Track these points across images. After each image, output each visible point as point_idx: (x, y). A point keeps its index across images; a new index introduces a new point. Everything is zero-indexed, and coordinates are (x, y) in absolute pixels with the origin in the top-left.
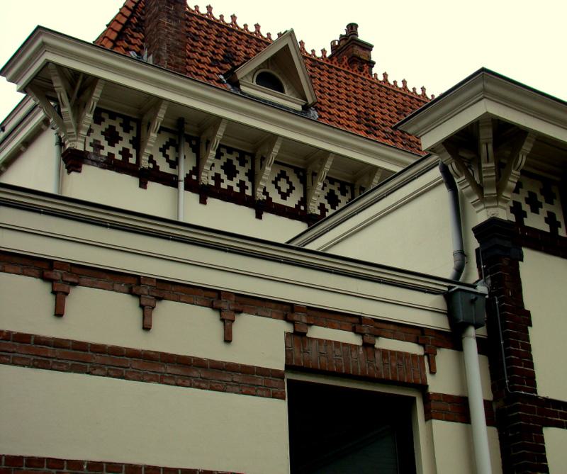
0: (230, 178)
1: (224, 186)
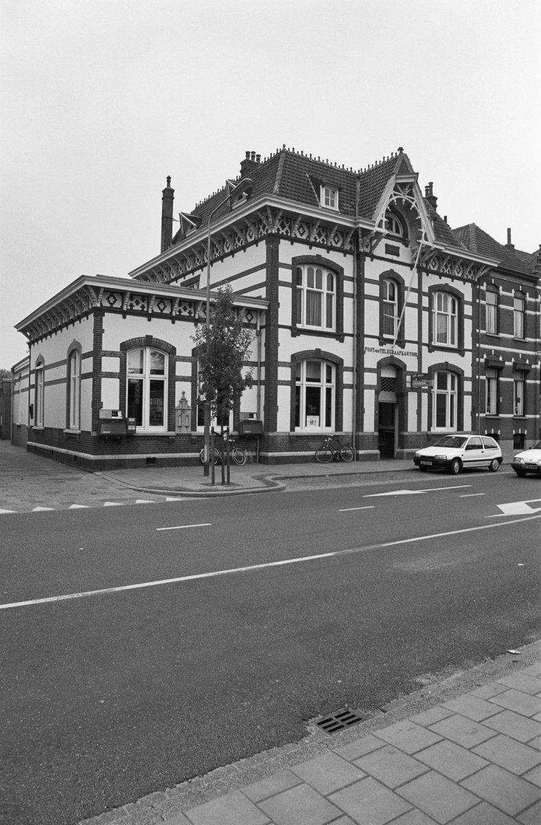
0: (283, 229)
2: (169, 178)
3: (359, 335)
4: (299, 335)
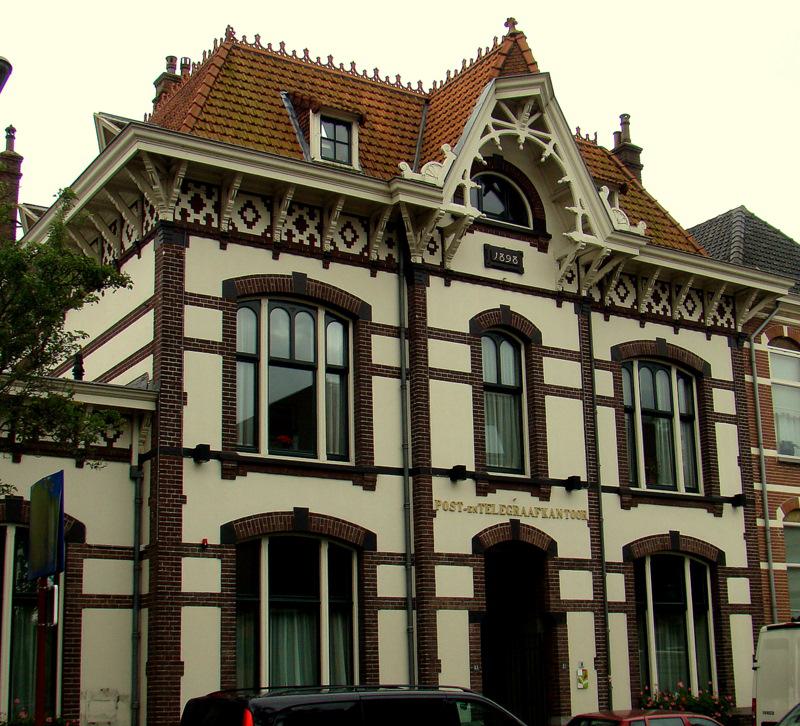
0: (197, 212)
1: (295, 240)
2: (11, 131)
3: (418, 471)
4: (636, 506)
